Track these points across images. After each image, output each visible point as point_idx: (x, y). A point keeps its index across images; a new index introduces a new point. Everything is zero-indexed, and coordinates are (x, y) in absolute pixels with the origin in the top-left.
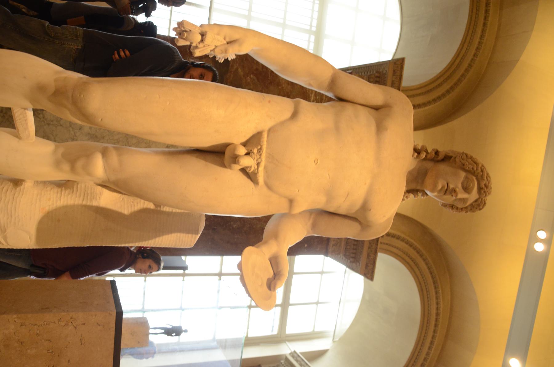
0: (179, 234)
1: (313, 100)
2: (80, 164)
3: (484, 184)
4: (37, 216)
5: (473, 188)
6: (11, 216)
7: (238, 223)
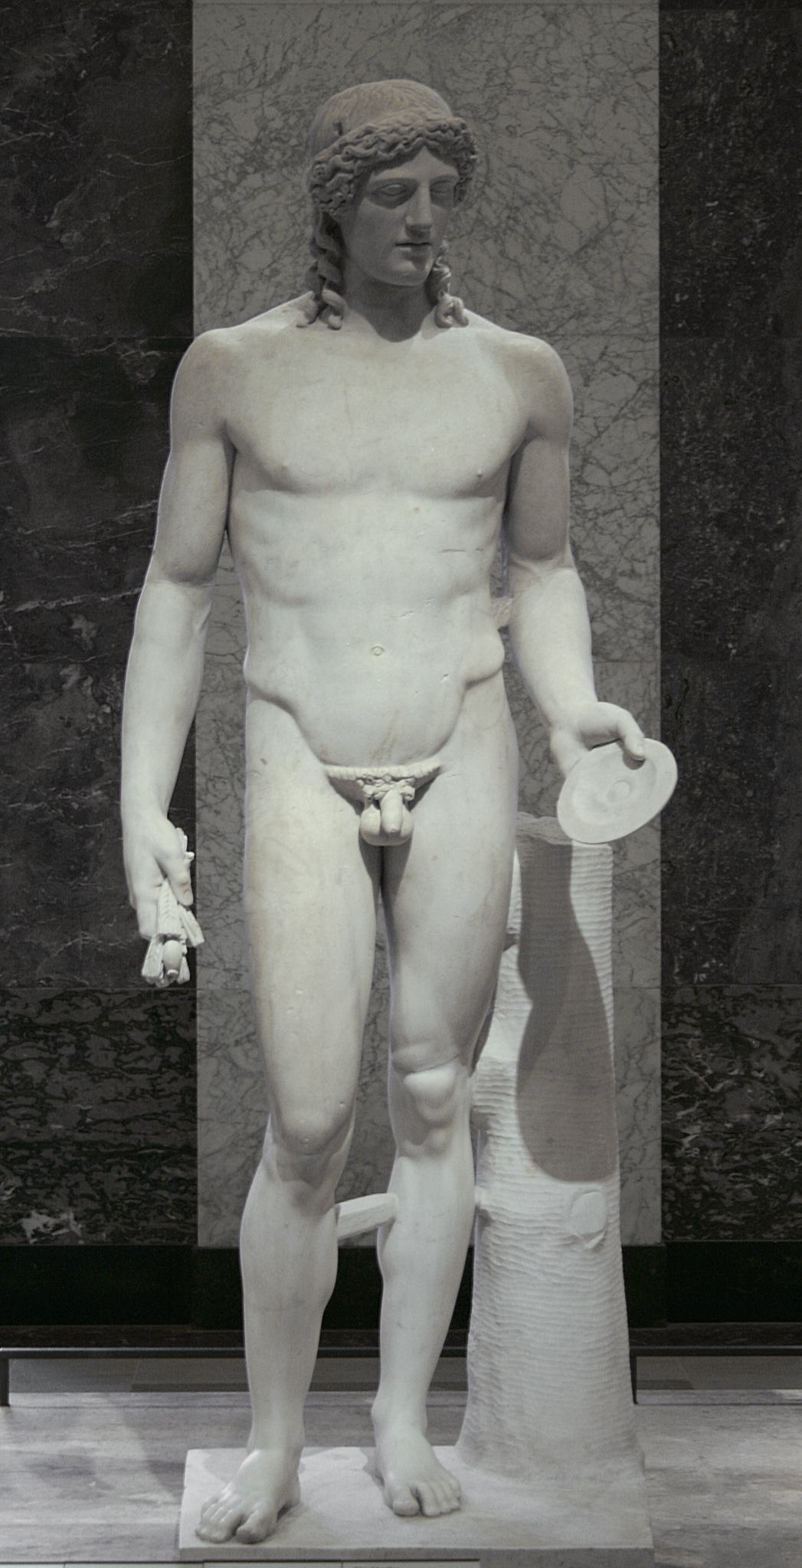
0: (573, 889)
2: (430, 1114)
4: (543, 1182)
5: (400, 181)
6: (544, 1228)
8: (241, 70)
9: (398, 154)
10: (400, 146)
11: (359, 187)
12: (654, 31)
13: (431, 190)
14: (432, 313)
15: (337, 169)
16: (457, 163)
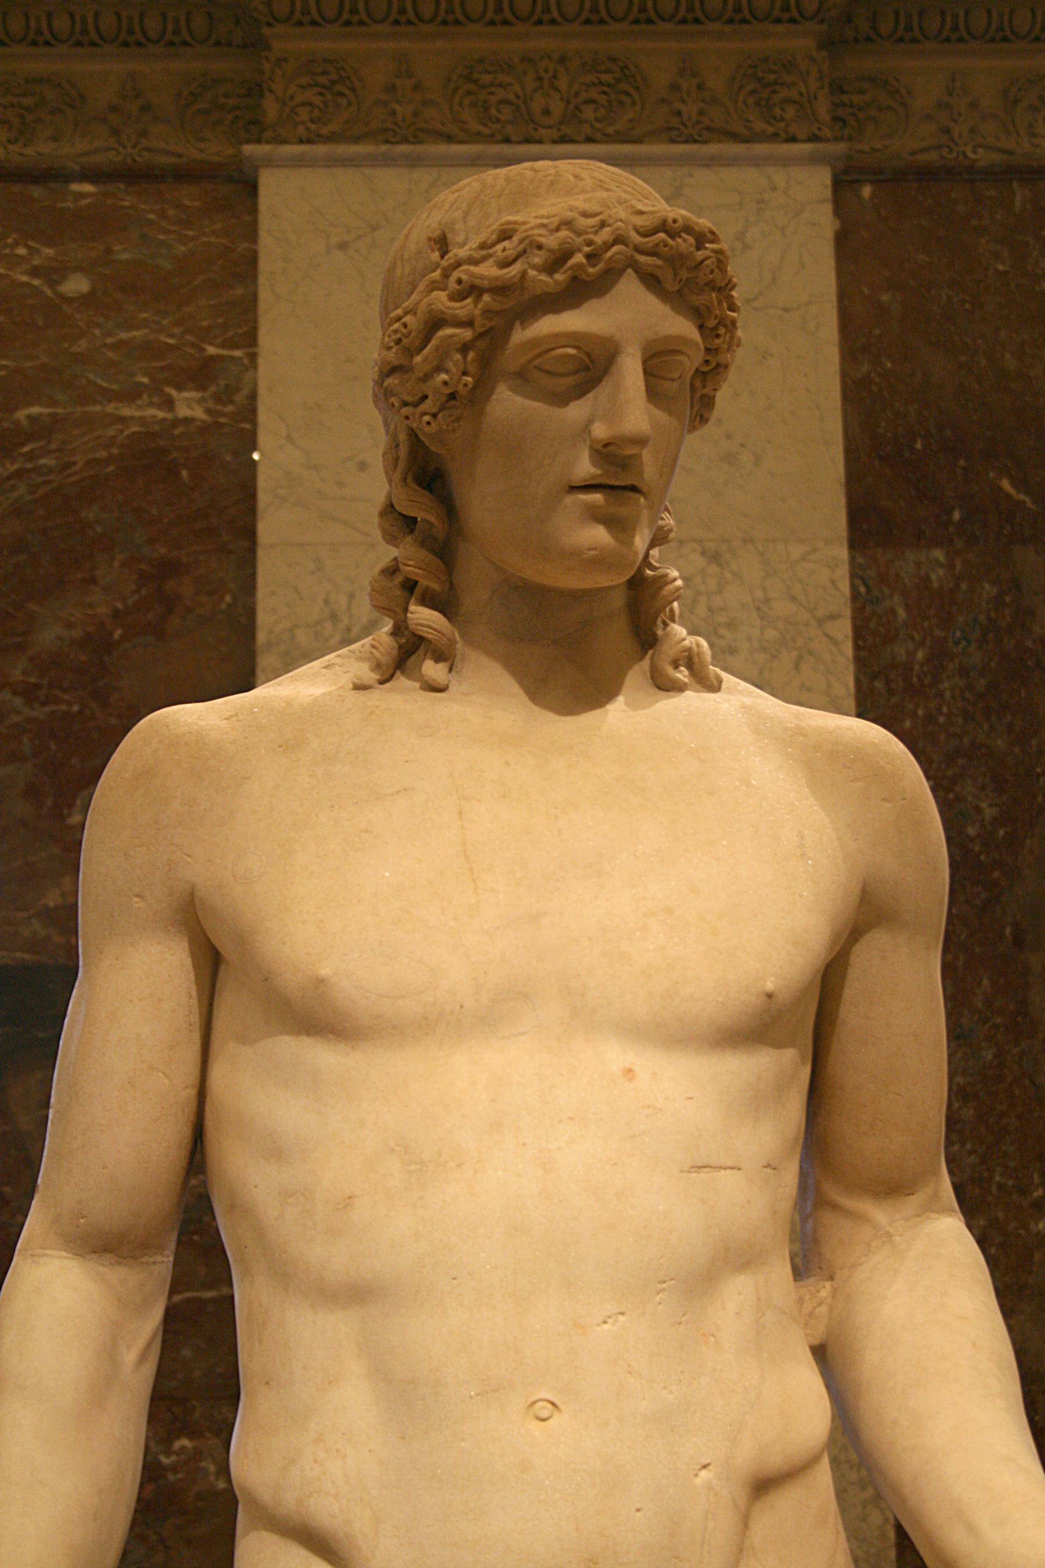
1: (159, 407)
3: (544, 277)
5: (575, 339)
7: (969, 790)
8: (319, 623)
9: (574, 279)
10: (579, 258)
11: (486, 362)
12: (843, 572)
13: (648, 373)
14: (646, 663)
15: (435, 323)
16: (699, 315)
